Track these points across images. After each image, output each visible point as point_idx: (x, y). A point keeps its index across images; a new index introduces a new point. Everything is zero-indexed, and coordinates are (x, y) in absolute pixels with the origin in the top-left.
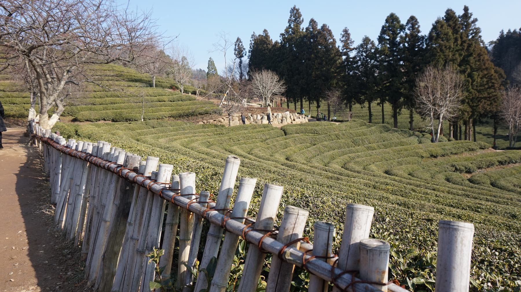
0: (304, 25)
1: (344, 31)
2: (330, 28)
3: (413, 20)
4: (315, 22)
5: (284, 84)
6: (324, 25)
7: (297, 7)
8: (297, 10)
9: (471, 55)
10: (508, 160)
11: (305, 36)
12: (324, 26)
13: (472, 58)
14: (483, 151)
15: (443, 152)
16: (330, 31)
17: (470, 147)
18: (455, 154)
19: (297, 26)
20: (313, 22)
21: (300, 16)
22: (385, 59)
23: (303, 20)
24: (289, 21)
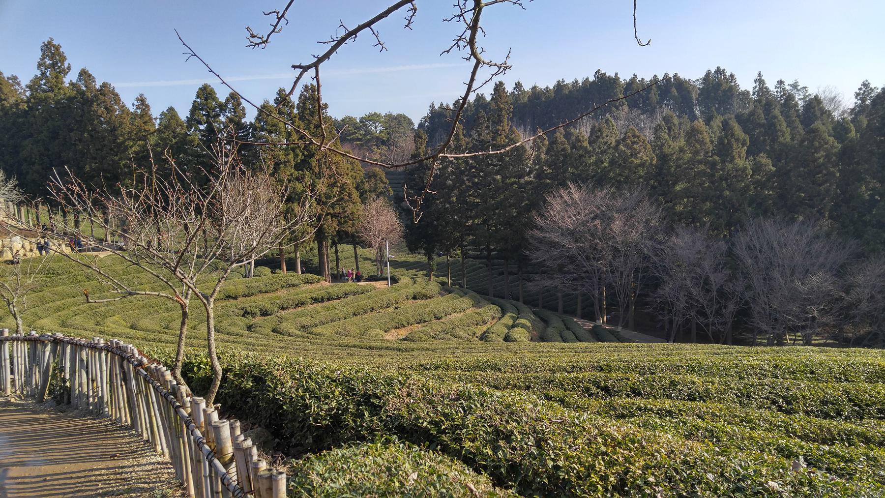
0: (71, 77)
1: (137, 100)
2: (116, 91)
3: (234, 97)
4: (90, 76)
5: (15, 186)
6: (104, 83)
7: (55, 43)
8: (57, 48)
9: (312, 155)
10: (326, 296)
11: (70, 99)
12: (104, 85)
13: (314, 159)
14: (309, 287)
15: (246, 291)
16: (117, 95)
17: (290, 282)
18: (266, 292)
19: (57, 78)
20: (84, 74)
21: (63, 59)
22: (674, 98)
23: (69, 68)
24: (40, 65)
